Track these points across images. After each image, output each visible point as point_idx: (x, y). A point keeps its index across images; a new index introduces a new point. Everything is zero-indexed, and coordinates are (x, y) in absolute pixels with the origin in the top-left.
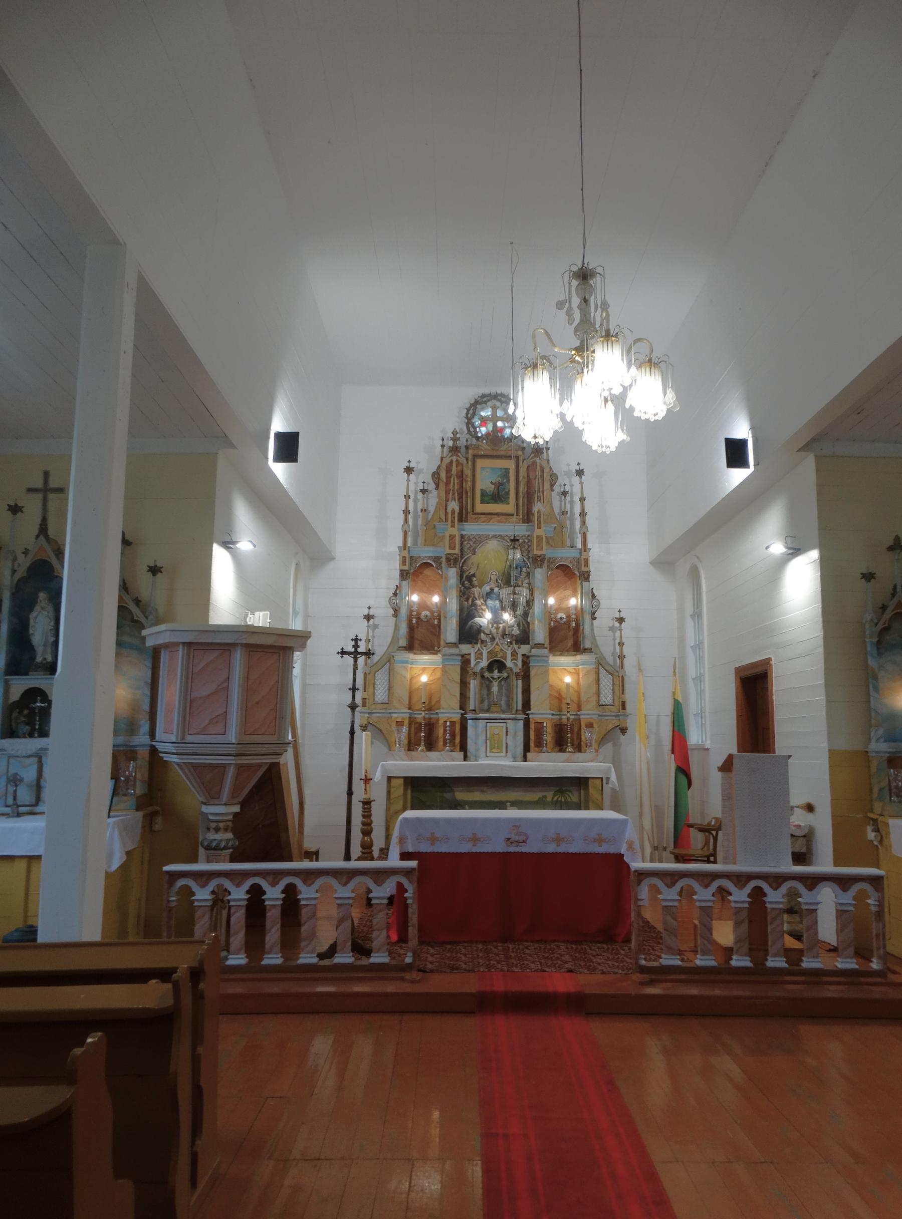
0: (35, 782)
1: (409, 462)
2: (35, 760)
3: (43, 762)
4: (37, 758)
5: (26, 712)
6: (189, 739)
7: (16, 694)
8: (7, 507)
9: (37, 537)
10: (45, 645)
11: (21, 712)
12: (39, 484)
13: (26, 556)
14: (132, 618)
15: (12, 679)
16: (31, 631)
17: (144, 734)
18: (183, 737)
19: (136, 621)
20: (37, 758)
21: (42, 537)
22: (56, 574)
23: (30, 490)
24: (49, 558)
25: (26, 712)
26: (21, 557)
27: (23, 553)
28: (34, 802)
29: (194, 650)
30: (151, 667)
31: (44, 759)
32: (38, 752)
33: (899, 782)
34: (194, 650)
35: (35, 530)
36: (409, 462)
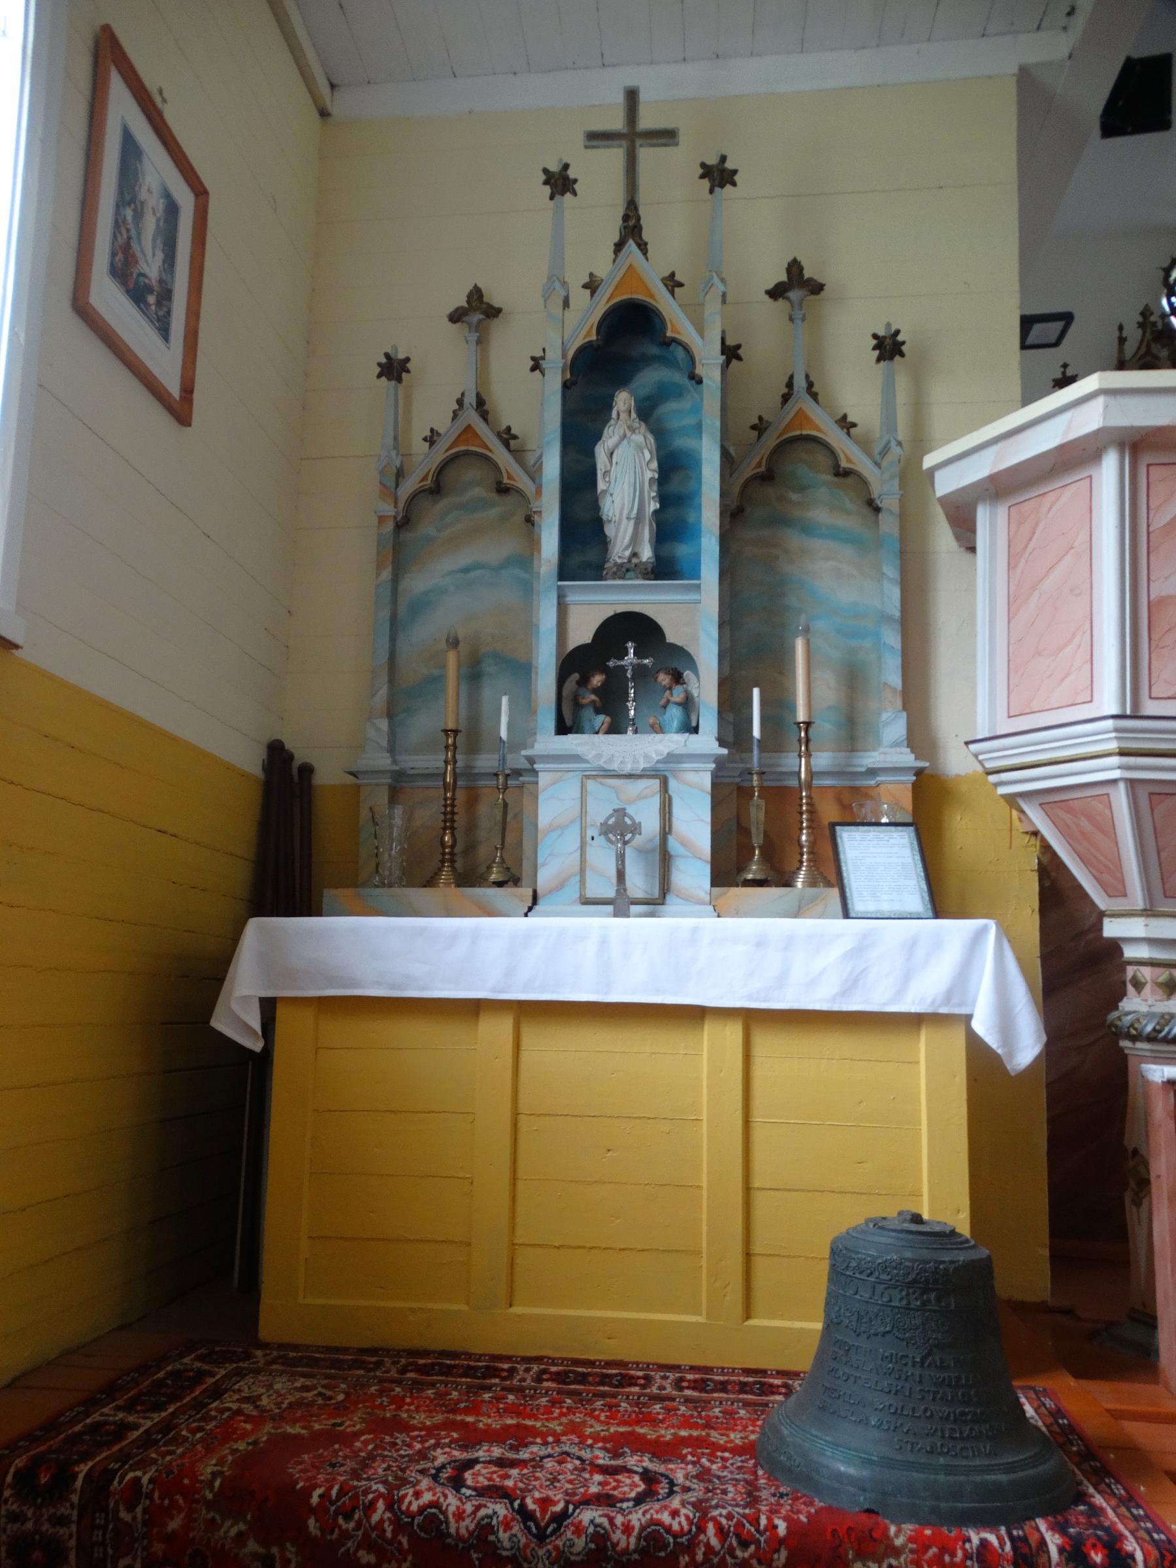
0: (657, 841)
1: (1065, 366)
2: (655, 784)
3: (670, 792)
4: (658, 780)
5: (597, 680)
6: (1150, 708)
7: (582, 632)
8: (543, 177)
9: (619, 247)
10: (638, 520)
11: (583, 682)
12: (617, 123)
13: (593, 294)
14: (837, 466)
15: (568, 586)
16: (601, 486)
17: (896, 744)
18: (1136, 703)
19: (847, 473)
20: (658, 780)
21: (631, 245)
22: (669, 334)
23: (596, 138)
24: (652, 296)
25: (597, 680)
26: (580, 297)
27: (585, 286)
28: (656, 894)
29: (1148, 465)
30: (899, 580)
31: (673, 784)
32: (660, 766)
33: (410, 1397)
34: (1148, 465)
35: (612, 231)
36: (1065, 366)
